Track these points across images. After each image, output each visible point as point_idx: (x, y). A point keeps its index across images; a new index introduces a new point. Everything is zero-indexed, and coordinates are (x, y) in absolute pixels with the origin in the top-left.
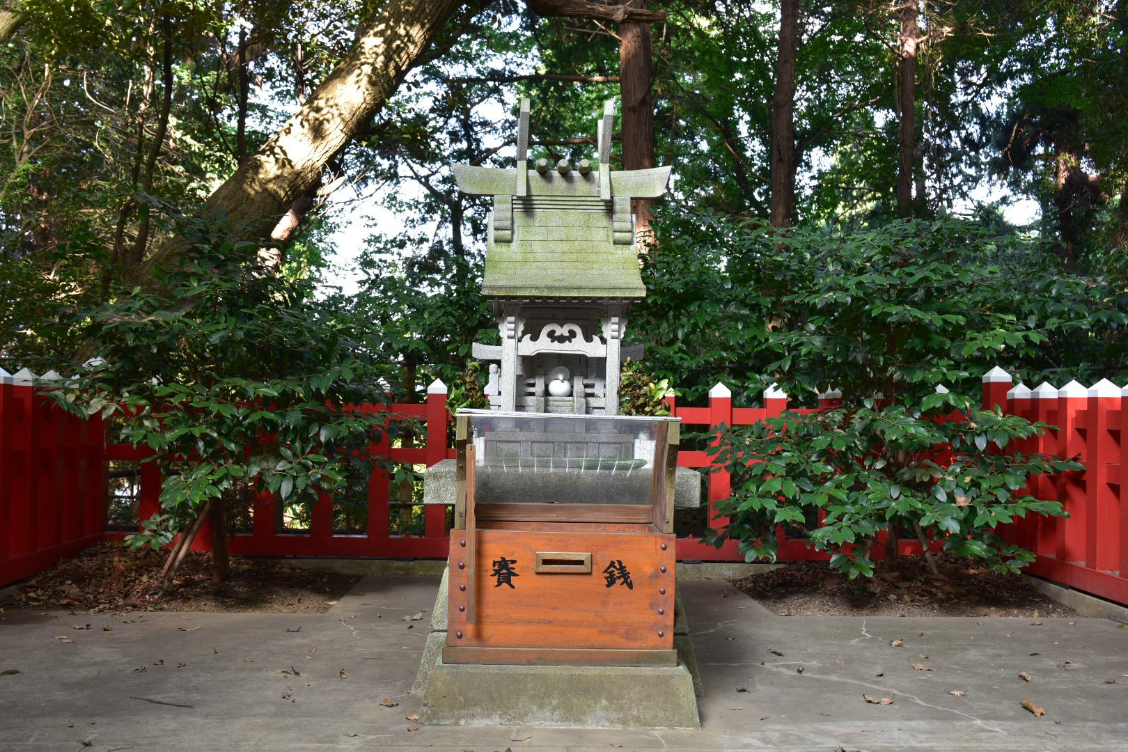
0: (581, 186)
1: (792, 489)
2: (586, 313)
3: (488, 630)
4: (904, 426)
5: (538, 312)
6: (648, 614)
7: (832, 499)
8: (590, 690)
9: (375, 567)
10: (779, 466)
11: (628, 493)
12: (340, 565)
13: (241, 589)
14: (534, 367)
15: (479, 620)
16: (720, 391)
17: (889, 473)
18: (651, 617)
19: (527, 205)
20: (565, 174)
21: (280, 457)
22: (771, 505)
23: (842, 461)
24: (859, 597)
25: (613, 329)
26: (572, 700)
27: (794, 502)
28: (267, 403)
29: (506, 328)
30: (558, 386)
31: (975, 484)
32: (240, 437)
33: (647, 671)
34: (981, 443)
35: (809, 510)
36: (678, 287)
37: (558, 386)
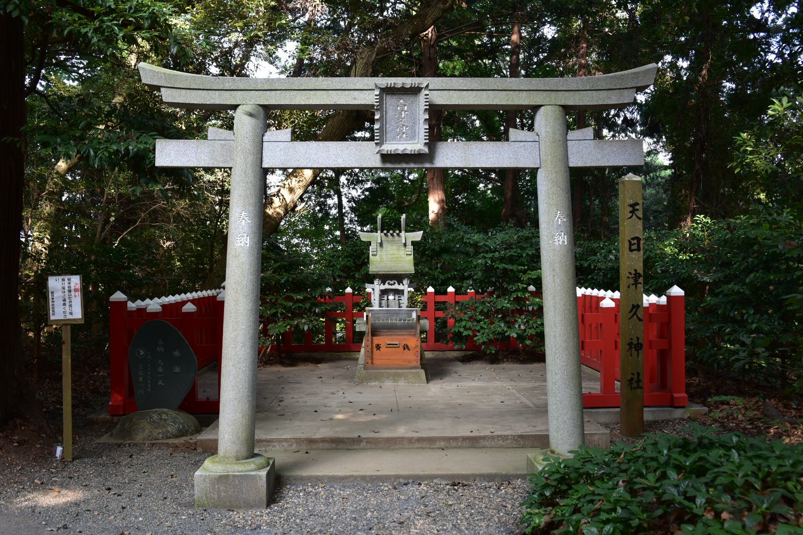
0: (397, 238)
1: (469, 324)
2: (399, 278)
3: (375, 362)
4: (505, 303)
5: (385, 278)
6: (413, 357)
7: (482, 328)
8: (400, 376)
9: (328, 355)
10: (466, 317)
11: (408, 328)
12: (316, 355)
13: (287, 362)
14: (384, 292)
15: (372, 359)
16: (451, 289)
17: (503, 318)
18: (414, 357)
19: (381, 244)
20: (392, 235)
21: (303, 318)
22: (462, 330)
23: (487, 315)
24: (494, 360)
25: (405, 282)
26: (396, 377)
27: (470, 329)
28: (299, 301)
29: (376, 282)
30: (391, 297)
31: (527, 322)
32: (292, 313)
33: (413, 371)
34: (530, 308)
35: (474, 331)
36: (437, 248)
37: (391, 297)
